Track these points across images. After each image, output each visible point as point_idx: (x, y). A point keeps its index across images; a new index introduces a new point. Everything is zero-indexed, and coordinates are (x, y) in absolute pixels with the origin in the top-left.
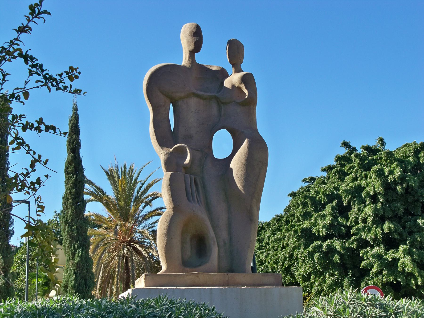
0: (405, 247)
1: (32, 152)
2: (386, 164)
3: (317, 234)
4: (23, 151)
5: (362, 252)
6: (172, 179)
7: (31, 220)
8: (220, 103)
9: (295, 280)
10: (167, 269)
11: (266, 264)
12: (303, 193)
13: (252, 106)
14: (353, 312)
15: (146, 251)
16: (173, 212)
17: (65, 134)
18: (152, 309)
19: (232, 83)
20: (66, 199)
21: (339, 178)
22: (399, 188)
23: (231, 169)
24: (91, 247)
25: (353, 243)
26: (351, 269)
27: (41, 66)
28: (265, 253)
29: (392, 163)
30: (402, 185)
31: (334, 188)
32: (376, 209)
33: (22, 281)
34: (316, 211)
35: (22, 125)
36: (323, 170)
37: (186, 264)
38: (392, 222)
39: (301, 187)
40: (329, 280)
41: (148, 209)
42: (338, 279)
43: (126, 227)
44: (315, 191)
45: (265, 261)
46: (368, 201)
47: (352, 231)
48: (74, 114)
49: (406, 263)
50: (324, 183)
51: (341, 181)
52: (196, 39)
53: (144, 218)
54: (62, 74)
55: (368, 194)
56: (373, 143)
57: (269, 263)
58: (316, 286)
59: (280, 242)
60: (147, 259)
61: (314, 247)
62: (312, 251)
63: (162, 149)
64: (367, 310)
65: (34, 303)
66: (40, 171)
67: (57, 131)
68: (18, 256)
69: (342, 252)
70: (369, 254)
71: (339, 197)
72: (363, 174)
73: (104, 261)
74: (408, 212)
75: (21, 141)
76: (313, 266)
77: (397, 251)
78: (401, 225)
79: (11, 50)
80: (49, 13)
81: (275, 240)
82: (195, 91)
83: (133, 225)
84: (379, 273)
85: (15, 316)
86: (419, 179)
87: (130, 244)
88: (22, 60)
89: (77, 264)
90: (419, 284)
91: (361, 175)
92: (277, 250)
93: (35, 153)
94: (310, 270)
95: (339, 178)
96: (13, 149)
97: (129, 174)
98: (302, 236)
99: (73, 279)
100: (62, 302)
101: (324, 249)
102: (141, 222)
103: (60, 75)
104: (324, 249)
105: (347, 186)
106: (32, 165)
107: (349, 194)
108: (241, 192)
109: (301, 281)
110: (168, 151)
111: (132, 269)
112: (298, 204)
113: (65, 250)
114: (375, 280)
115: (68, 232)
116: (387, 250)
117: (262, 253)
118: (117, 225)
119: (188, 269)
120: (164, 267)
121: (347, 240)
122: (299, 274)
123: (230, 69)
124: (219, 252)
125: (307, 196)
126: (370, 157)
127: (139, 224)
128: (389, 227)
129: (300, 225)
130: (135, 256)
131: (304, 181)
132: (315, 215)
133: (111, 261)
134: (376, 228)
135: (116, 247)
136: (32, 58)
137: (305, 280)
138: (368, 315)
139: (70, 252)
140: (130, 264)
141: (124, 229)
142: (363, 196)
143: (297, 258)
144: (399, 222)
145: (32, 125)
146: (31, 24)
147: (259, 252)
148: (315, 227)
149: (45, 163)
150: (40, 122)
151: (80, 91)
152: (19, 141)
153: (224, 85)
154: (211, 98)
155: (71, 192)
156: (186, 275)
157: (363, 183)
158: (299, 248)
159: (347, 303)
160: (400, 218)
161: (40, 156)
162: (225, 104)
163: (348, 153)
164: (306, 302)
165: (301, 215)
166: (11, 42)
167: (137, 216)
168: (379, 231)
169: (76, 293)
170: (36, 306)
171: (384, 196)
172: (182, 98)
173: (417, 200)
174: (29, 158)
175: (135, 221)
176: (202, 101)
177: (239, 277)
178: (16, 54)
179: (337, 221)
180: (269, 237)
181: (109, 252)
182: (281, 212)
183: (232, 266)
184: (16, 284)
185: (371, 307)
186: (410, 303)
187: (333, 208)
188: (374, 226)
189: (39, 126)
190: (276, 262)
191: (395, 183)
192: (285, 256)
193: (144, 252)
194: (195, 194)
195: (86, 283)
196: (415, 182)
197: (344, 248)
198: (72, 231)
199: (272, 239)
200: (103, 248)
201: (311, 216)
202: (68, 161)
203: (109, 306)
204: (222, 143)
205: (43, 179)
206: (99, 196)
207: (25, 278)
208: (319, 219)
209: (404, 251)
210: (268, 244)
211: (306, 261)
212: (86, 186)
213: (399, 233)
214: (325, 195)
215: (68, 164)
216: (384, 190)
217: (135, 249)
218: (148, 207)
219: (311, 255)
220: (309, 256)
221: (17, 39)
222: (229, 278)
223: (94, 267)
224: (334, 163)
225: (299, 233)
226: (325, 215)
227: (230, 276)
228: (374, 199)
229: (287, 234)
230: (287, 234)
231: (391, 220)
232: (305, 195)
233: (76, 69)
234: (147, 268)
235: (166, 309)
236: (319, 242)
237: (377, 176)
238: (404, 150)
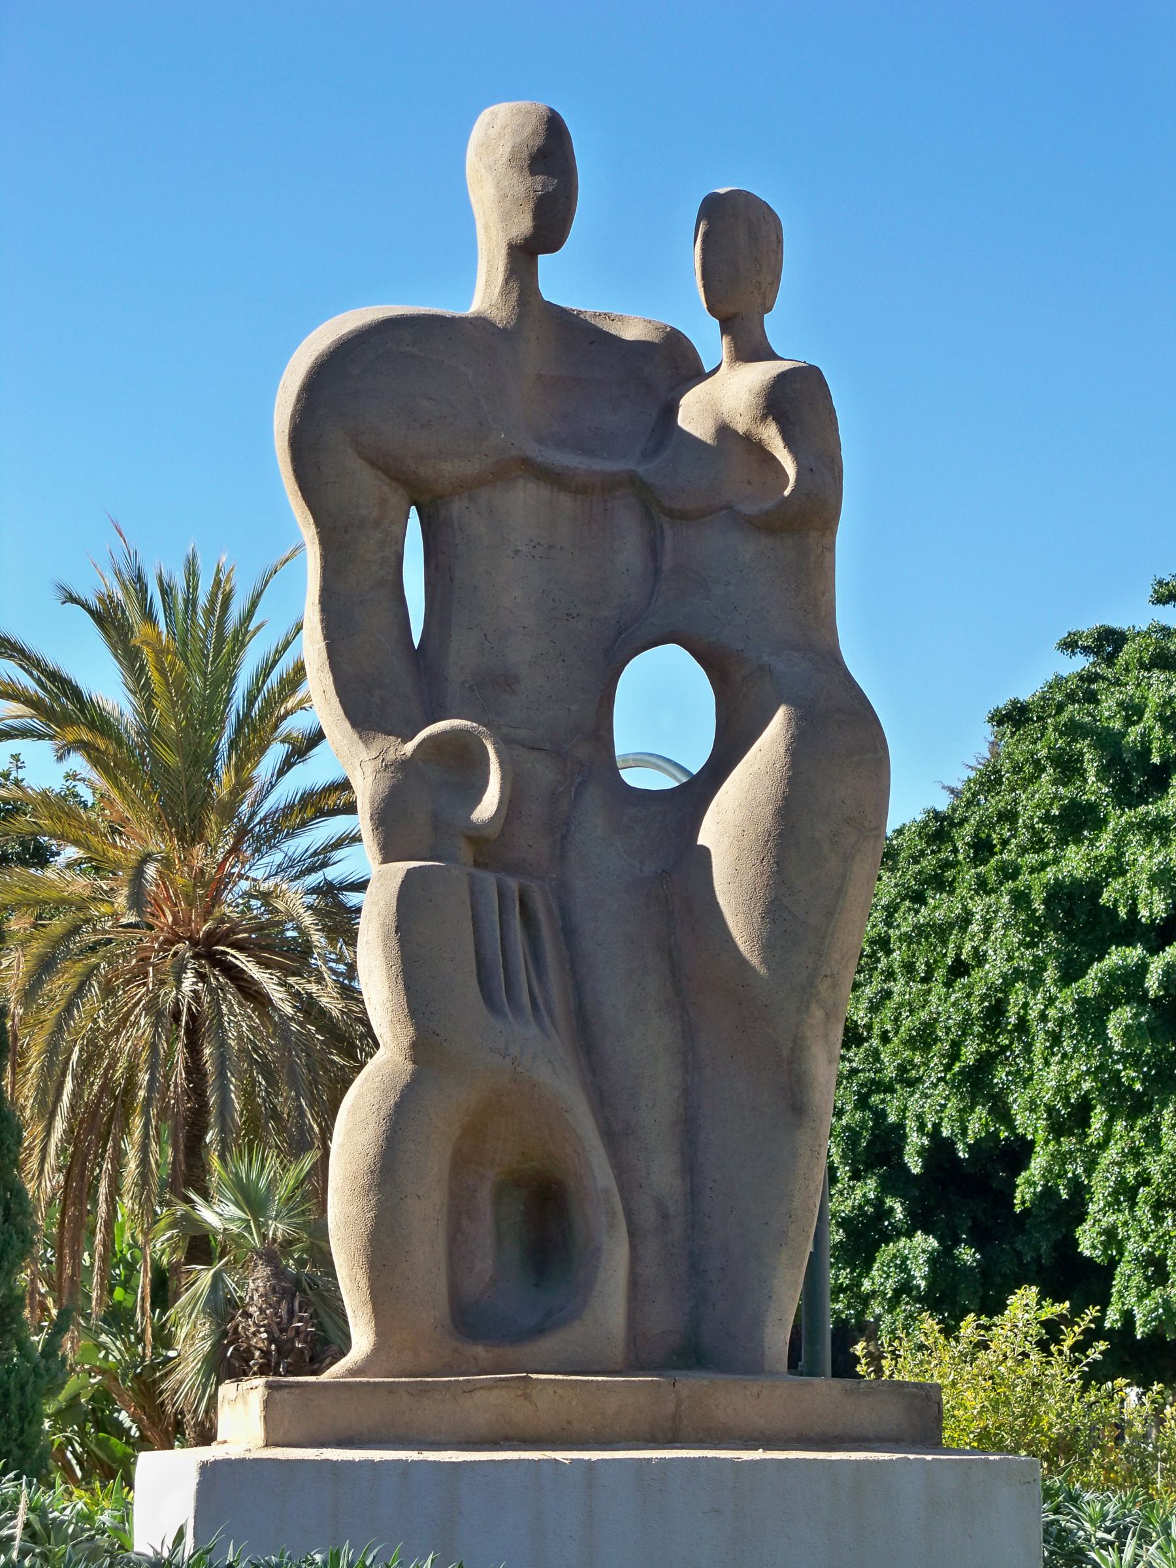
3: (1122, 912)
8: (656, 511)
10: (378, 1348)
11: (875, 1042)
12: (1060, 708)
13: (814, 534)
16: (409, 1066)
19: (717, 415)
23: (705, 852)
28: (868, 991)
34: (1126, 797)
39: (1051, 677)
43: (191, 868)
44: (1120, 704)
45: (869, 1027)
52: (544, 185)
57: (885, 1038)
58: (1113, 1163)
59: (945, 943)
60: (294, 1027)
61: (1111, 974)
62: (1097, 998)
63: (366, 741)
76: (1101, 1068)
81: (920, 930)
82: (533, 450)
83: (225, 859)
92: (926, 980)
94: (1086, 1086)
97: (209, 612)
101: (1152, 983)
104: (1152, 983)
108: (753, 969)
109: (1041, 1136)
110: (391, 756)
111: (221, 1075)
112: (1037, 763)
118: (147, 858)
119: (479, 1350)
120: (362, 1338)
122: (1032, 1101)
123: (709, 340)
124: (635, 1258)
127: (258, 850)
129: (1043, 866)
131: (1070, 645)
132: (1117, 819)
133: (117, 1032)
135: (144, 960)
137: (1057, 1129)
140: (207, 1051)
141: (182, 878)
143: (1022, 1026)
148: (1115, 876)
153: (680, 422)
154: (609, 485)
156: (470, 1389)
158: (1034, 980)
162: (681, 516)
164: (1061, 1353)
165: (1047, 819)
172: (468, 486)
176: (565, 501)
177: (733, 1398)
180: (891, 910)
181: (108, 990)
183: (692, 1343)
190: (923, 1038)
192: (968, 1013)
193: (277, 994)
194: (521, 954)
199: (906, 923)
200: (79, 968)
201: (1100, 824)
204: (661, 709)
211: (1068, 1046)
219: (1092, 1015)
220: (1082, 1022)
222: (679, 1402)
225: (1039, 907)
226: (1164, 819)
227: (685, 1393)
229: (978, 907)
230: (978, 907)
232: (1071, 719)
234: (292, 1072)
236: (1136, 953)
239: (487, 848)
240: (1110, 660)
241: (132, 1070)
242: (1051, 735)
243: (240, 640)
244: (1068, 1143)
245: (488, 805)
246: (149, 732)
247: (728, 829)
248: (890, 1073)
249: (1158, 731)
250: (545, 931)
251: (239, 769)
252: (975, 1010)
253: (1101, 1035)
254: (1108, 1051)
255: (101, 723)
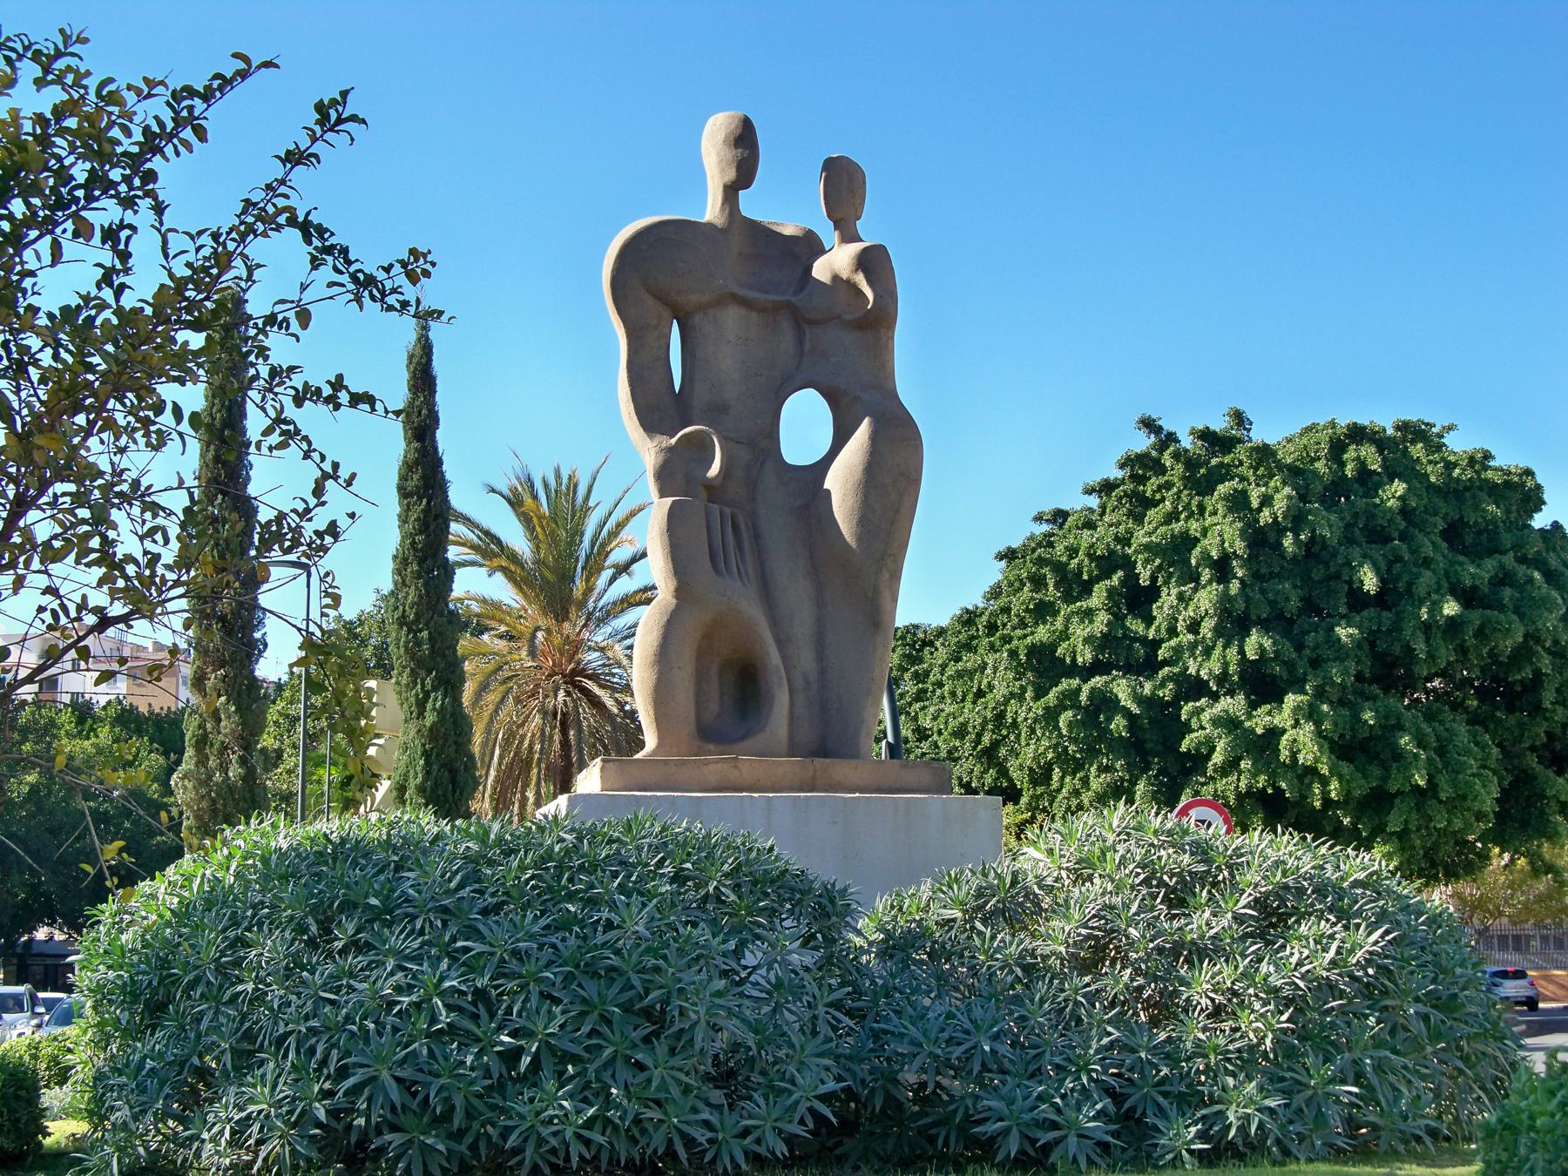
0: (1300, 698)
1: (316, 456)
2: (1252, 479)
3: (1068, 660)
4: (295, 450)
5: (1187, 708)
6: (673, 515)
7: (313, 628)
8: (801, 321)
9: (1010, 780)
10: (658, 746)
11: (935, 737)
12: (1034, 550)
14: (1123, 862)
15: (616, 700)
17: (397, 413)
18: (615, 846)
20: (401, 562)
21: (1130, 514)
22: (1288, 542)
23: (828, 492)
24: (469, 689)
25: (1162, 685)
26: (1157, 757)
27: (345, 251)
28: (932, 709)
29: (1271, 476)
30: (1296, 535)
31: (1117, 539)
32: (1225, 598)
33: (289, 772)
34: (1069, 598)
35: (293, 392)
36: (1089, 491)
37: (709, 734)
38: (1267, 632)
40: (1097, 783)
41: (625, 585)
42: (1122, 779)
46: (1206, 574)
47: (1162, 653)
48: (419, 340)
49: (1303, 743)
50: (1090, 525)
51: (1135, 520)
53: (608, 613)
54: (391, 266)
55: (1205, 556)
56: (1219, 424)
63: (651, 438)
64: (1160, 858)
65: (321, 826)
66: (337, 502)
67: (378, 406)
68: (280, 705)
69: (1135, 709)
70: (1206, 716)
71: (1128, 564)
72: (1194, 503)
73: (497, 722)
74: (1310, 607)
75: (291, 427)
76: (1056, 746)
77: (1280, 709)
78: (1291, 640)
79: (271, 209)
80: (364, 122)
81: (959, 675)
84: (1231, 766)
85: (274, 857)
86: (1342, 519)
87: (574, 678)
88: (297, 233)
89: (431, 729)
90: (1333, 795)
91: (1187, 507)
92: (963, 701)
93: (323, 458)
94: (1050, 756)
95: (1130, 514)
96: (271, 448)
98: (1029, 666)
99: (419, 769)
100: (391, 825)
101: (1083, 697)
102: (602, 621)
103: (387, 269)
104: (1083, 697)
105: (1150, 534)
106: (318, 491)
107: (1156, 556)
113: (400, 693)
114: (1220, 785)
115: (406, 647)
116: (1253, 706)
117: (924, 708)
118: (538, 629)
119: (711, 746)
120: (650, 739)
121: (1148, 678)
123: (827, 232)
125: (1045, 560)
126: (1215, 457)
128: (1261, 645)
129: (1025, 636)
130: (585, 710)
131: (1039, 518)
132: (1065, 609)
133: (523, 725)
134: (1225, 647)
135: (537, 686)
136: (321, 230)
137: (1034, 782)
138: (1162, 868)
139: (412, 700)
141: (557, 640)
142: (1193, 562)
143: (1015, 723)
144: (1287, 634)
145: (319, 390)
146: (319, 148)
147: (917, 706)
149: (349, 483)
150: (338, 384)
151: (441, 313)
152: (284, 427)
154: (777, 307)
155: (413, 543)
156: (707, 763)
157: (1194, 527)
158: (1021, 697)
159: (1111, 838)
160: (1291, 622)
161: (336, 466)
163: (1153, 447)
165: (1027, 610)
166: (269, 187)
167: (591, 604)
168: (1232, 653)
169: (426, 805)
170: (325, 835)
171: (1248, 562)
172: (703, 308)
173: (1337, 576)
174: (311, 472)
175: (588, 619)
176: (754, 316)
177: (841, 769)
178: (282, 220)
179: (1123, 627)
180: (944, 667)
181: (518, 701)
182: (975, 599)
183: (827, 740)
184: (275, 781)
185: (1171, 851)
186: (1271, 841)
187: (1111, 592)
188: (1220, 644)
189: (336, 394)
190: (960, 733)
191: (1277, 528)
195: (454, 782)
196: (1330, 526)
197: (1139, 699)
198: (418, 643)
199: (950, 671)
200: (502, 688)
201: (1055, 613)
202: (405, 462)
203: (508, 837)
204: (804, 424)
205: (343, 522)
206: (490, 549)
207: (296, 766)
208: (1075, 619)
209: (1297, 709)
210: (940, 685)
212: (455, 527)
213: (1285, 663)
214: (1091, 556)
215: (408, 468)
216: (1248, 546)
217: (586, 692)
218: (624, 578)
219: (1051, 715)
221: (282, 182)
223: (477, 739)
224: (1116, 474)
225: (1023, 658)
228: (1222, 569)
231: (1266, 626)
233: (425, 256)
235: (650, 846)
236: (1075, 682)
237: (1230, 510)
238: (1305, 441)
239: (713, 491)
240: (1061, 527)
241: (531, 747)
242: (1029, 565)
243: (586, 510)
244: (1040, 790)
245: (715, 469)
246: (537, 562)
247: (840, 482)
248: (943, 754)
249: (1086, 561)
250: (745, 535)
251: (588, 580)
252: (989, 715)
253: (1057, 728)
254: (1060, 736)
255: (513, 557)
